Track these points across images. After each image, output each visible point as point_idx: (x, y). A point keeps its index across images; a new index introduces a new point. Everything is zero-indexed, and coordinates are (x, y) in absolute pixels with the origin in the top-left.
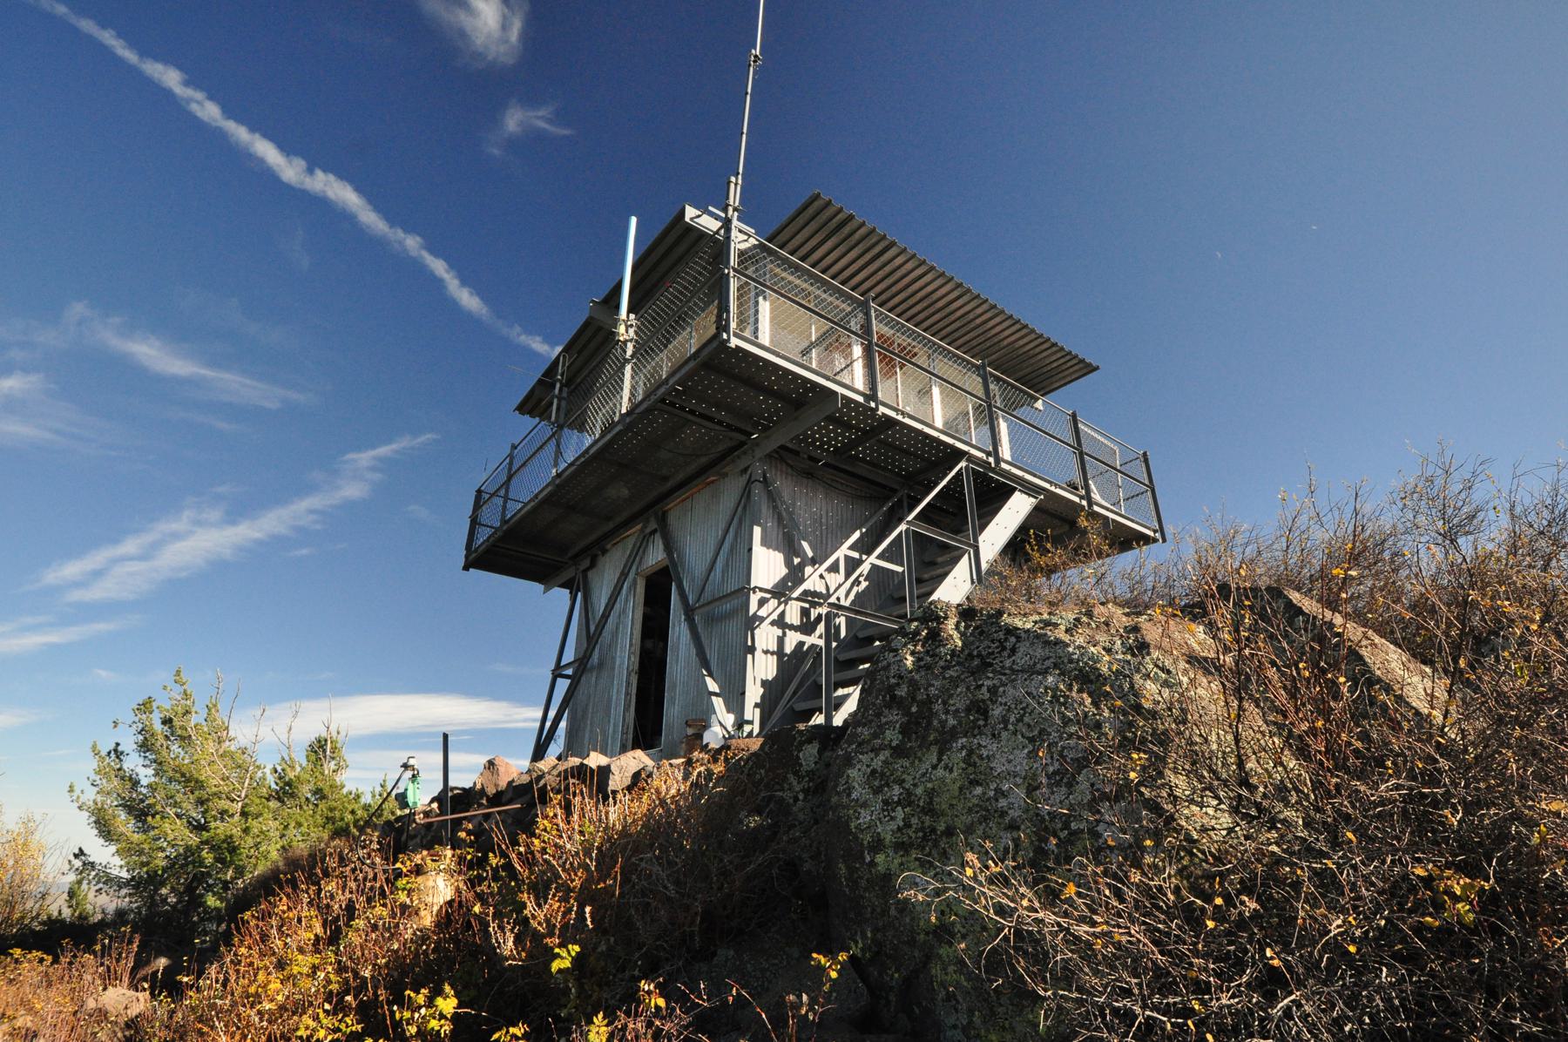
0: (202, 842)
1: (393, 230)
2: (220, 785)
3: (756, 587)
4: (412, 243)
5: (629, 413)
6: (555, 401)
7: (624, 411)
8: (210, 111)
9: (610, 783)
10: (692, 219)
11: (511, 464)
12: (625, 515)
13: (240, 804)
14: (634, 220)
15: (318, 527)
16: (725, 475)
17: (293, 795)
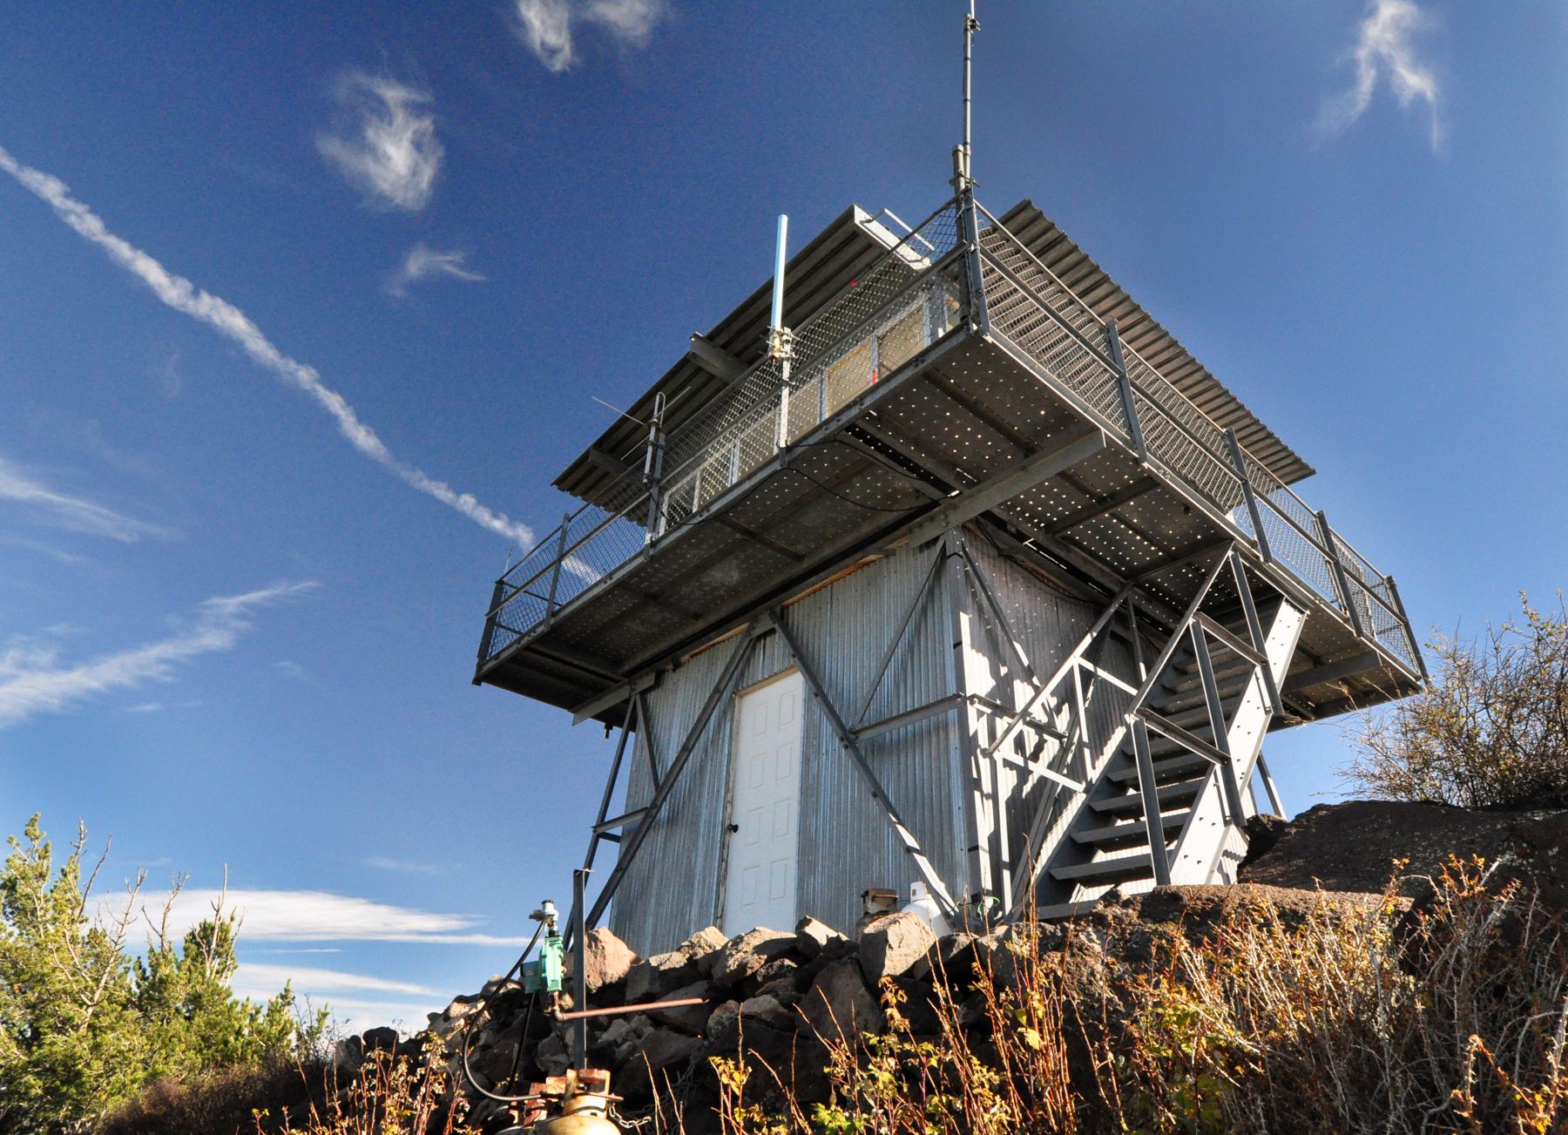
0: (29, 1062)
1: (282, 361)
2: (69, 981)
3: (974, 696)
4: (305, 376)
5: (789, 449)
6: (650, 449)
7: (783, 445)
8: (90, 225)
9: (887, 962)
10: (862, 222)
11: (563, 539)
12: (724, 611)
13: (90, 1010)
14: (784, 220)
15: (169, 679)
16: (889, 554)
17: (162, 1003)
